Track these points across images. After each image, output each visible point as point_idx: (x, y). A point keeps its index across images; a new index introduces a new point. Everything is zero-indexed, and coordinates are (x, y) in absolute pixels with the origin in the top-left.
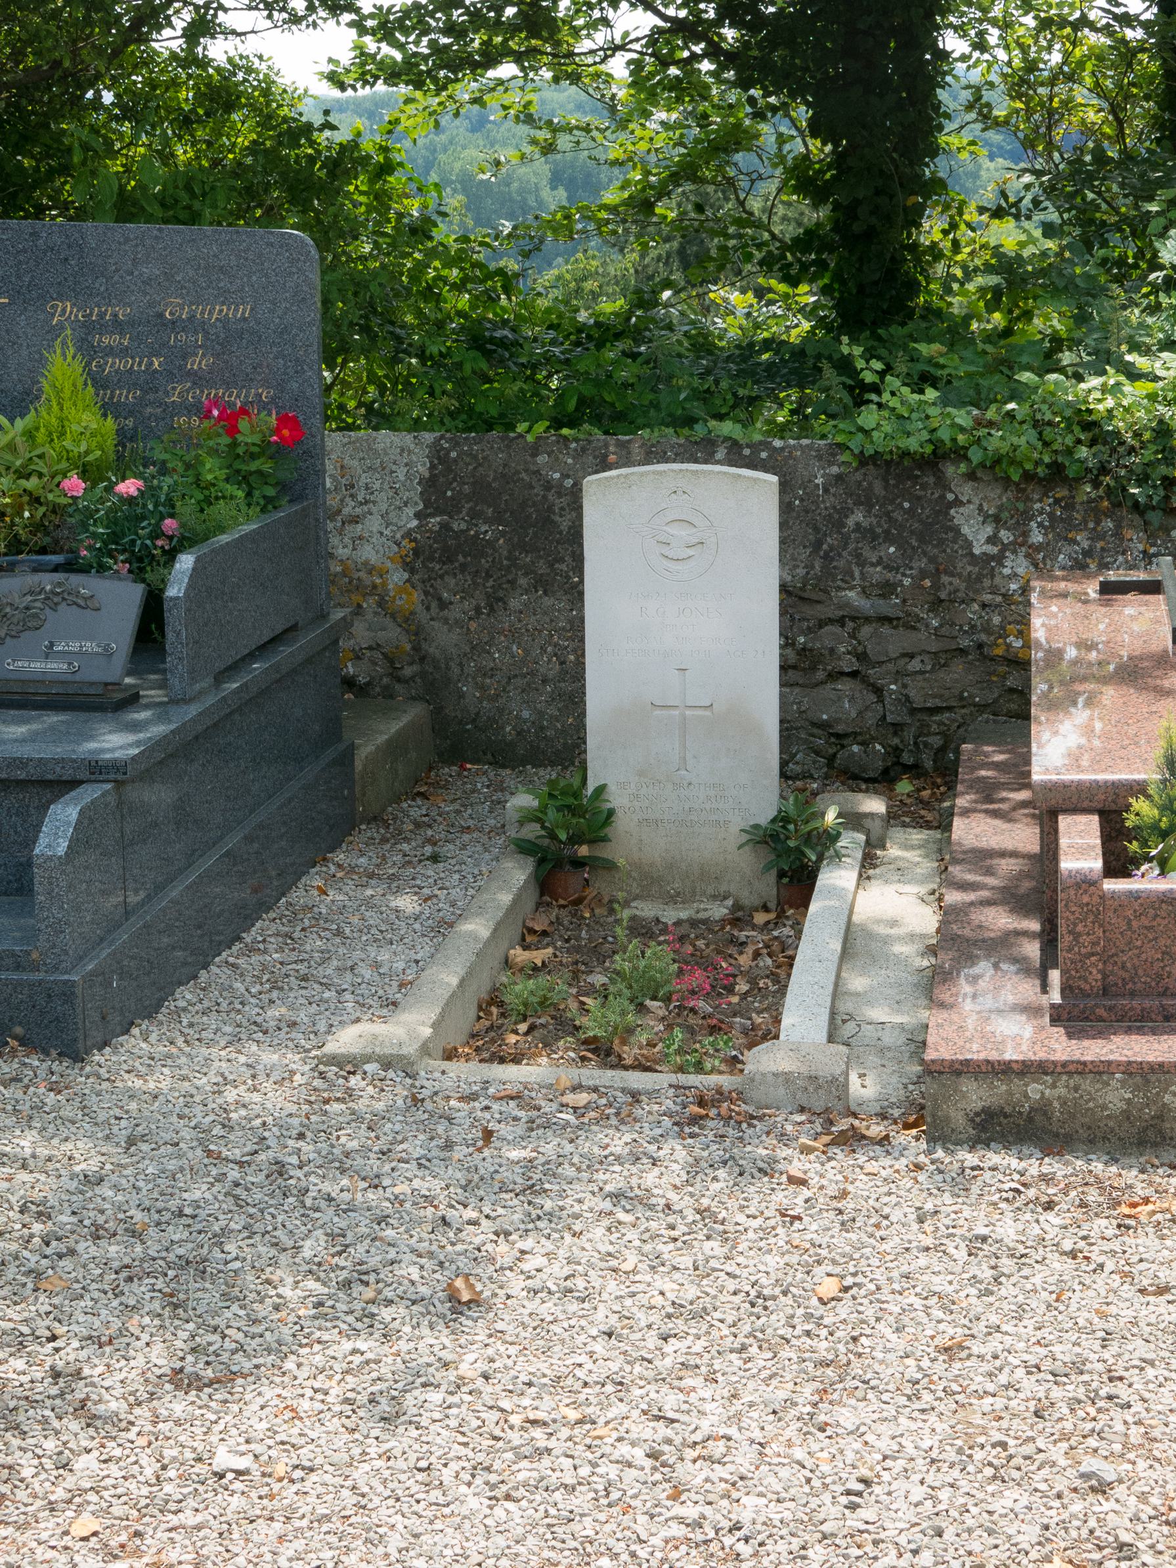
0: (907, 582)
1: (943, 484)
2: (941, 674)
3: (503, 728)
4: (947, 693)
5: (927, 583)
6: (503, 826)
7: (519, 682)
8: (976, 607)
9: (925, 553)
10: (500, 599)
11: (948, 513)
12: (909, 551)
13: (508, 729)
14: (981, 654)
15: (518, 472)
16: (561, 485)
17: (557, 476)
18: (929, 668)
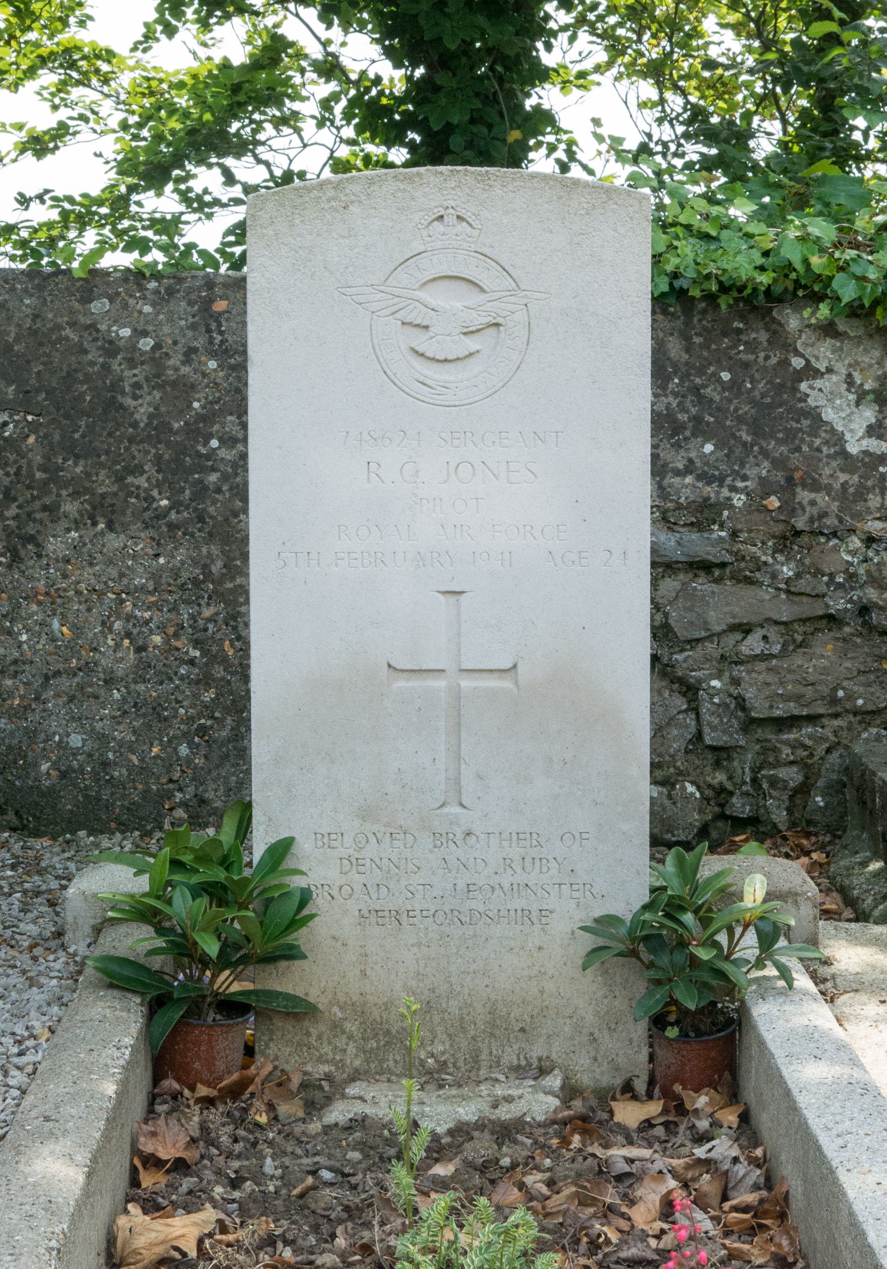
0: (739, 500)
1: (781, 341)
2: (798, 660)
3: (36, 765)
4: (809, 692)
5: (774, 502)
6: (59, 934)
7: (65, 683)
8: (856, 542)
9: (765, 454)
10: (31, 539)
11: (795, 390)
12: (738, 451)
13: (44, 767)
14: (865, 624)
15: (58, 327)
16: (134, 348)
17: (126, 332)
18: (776, 649)
